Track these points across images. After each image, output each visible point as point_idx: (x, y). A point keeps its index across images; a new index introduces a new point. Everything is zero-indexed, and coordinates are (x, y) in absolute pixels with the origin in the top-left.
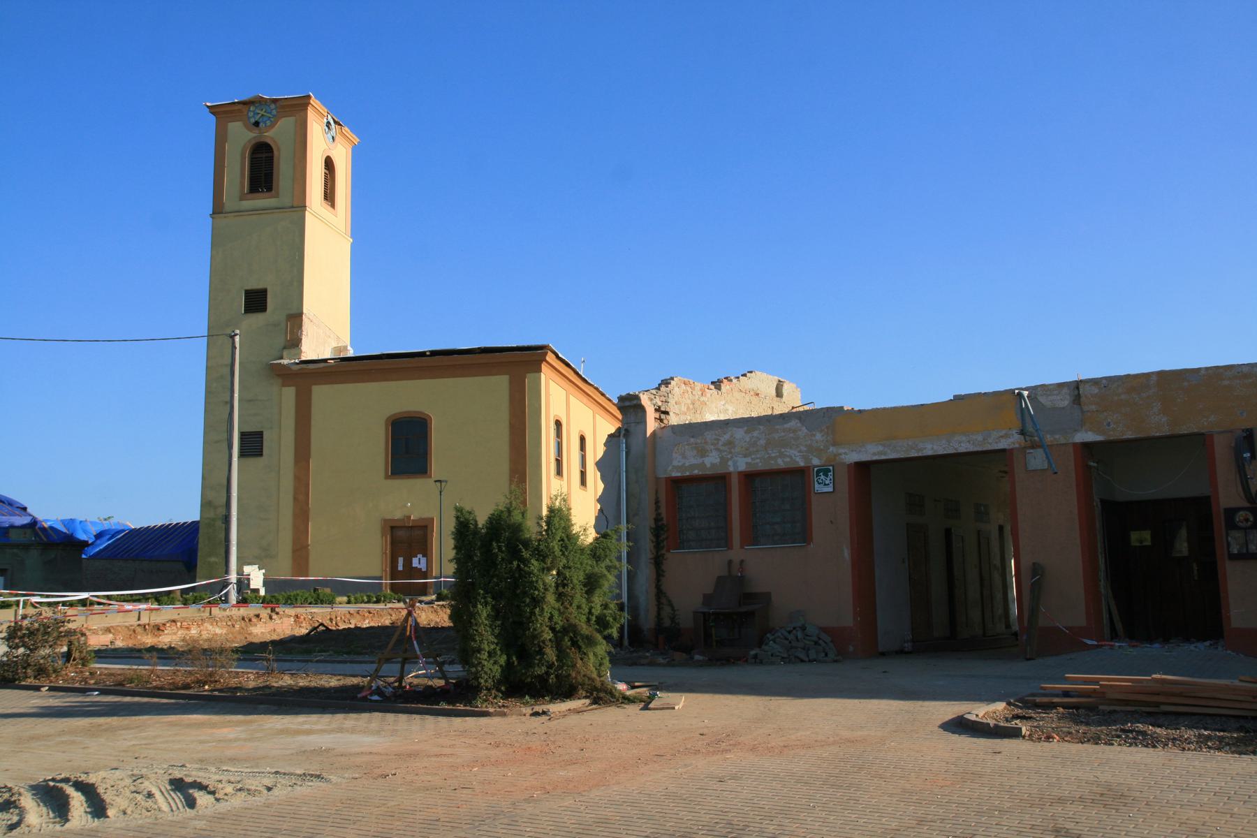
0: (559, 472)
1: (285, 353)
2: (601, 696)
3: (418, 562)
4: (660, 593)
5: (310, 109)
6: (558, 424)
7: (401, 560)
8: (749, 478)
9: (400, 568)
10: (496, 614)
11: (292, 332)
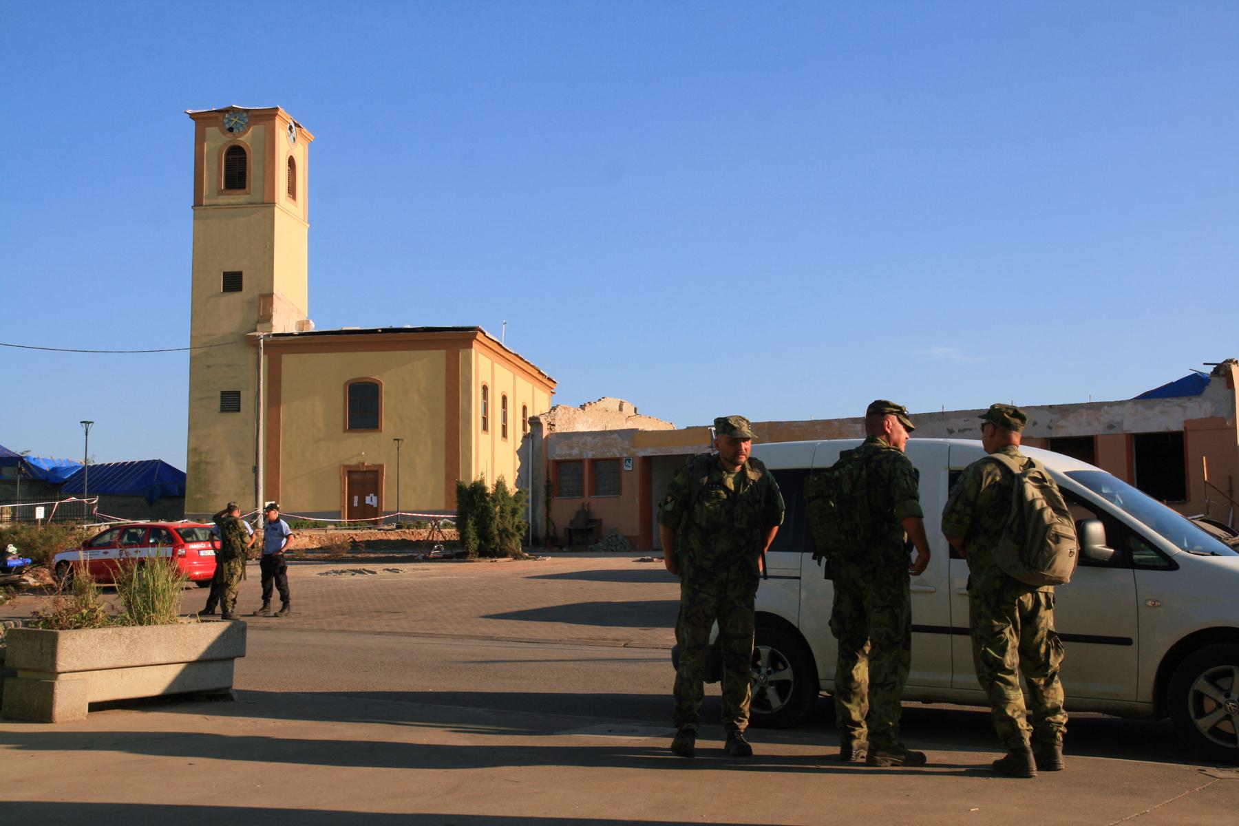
0: (485, 428)
1: (259, 327)
2: (517, 557)
3: (371, 500)
4: (548, 519)
5: (277, 118)
6: (485, 388)
7: (356, 498)
8: (594, 462)
9: (356, 504)
10: (475, 524)
11: (264, 308)
